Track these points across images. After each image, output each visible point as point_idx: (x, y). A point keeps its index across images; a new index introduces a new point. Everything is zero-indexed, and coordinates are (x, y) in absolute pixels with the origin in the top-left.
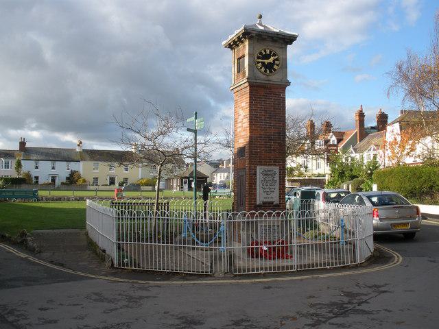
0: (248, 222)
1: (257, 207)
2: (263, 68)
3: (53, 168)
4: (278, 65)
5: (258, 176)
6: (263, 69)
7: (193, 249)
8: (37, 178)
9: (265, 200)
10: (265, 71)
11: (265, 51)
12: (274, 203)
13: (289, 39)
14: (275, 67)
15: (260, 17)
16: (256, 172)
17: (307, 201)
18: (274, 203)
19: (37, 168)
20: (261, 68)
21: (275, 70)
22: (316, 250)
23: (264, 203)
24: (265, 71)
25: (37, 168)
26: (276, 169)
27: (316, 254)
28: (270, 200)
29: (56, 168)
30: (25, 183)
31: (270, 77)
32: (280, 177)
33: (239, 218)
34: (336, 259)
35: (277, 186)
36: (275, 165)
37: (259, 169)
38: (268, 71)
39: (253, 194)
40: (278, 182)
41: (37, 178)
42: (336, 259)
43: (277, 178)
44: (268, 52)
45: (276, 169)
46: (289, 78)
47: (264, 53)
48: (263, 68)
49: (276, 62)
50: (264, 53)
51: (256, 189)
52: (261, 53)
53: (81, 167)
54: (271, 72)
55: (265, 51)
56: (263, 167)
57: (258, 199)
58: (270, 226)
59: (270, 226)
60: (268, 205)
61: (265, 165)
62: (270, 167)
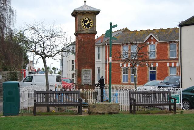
7: (107, 89)
10: (86, 28)
11: (86, 19)
13: (98, 13)
15: (85, 2)
20: (84, 27)
24: (86, 28)
30: (11, 8)
34: (123, 101)
38: (87, 28)
42: (123, 101)
44: (87, 19)
46: (97, 30)
47: (85, 20)
49: (91, 23)
50: (85, 20)
52: (84, 20)
53: (37, 97)
54: (88, 28)
55: (86, 19)
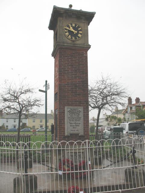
0: (59, 151)
1: (68, 138)
2: (70, 36)
3: (15, 122)
4: (81, 34)
5: (66, 114)
6: (70, 37)
8: (7, 126)
9: (72, 132)
10: (72, 38)
12: (79, 135)
13: (88, 17)
14: (79, 35)
16: (64, 110)
17: (117, 134)
18: (79, 135)
19: (7, 122)
20: (68, 36)
21: (79, 37)
22: (77, 178)
23: (71, 135)
24: (72, 38)
25: (7, 122)
26: (81, 109)
27: (81, 182)
28: (76, 132)
29: (8, 122)
31: (75, 42)
32: (84, 115)
33: (106, 144)
35: (81, 122)
36: (80, 106)
37: (67, 109)
38: (73, 38)
39: (62, 129)
40: (82, 118)
41: (7, 126)
43: (81, 115)
45: (81, 109)
48: (70, 36)
51: (64, 124)
54: (76, 38)
56: (70, 107)
57: (66, 132)
58: (75, 153)
59: (75, 153)
60: (74, 136)
61: (71, 105)
62: (76, 107)
